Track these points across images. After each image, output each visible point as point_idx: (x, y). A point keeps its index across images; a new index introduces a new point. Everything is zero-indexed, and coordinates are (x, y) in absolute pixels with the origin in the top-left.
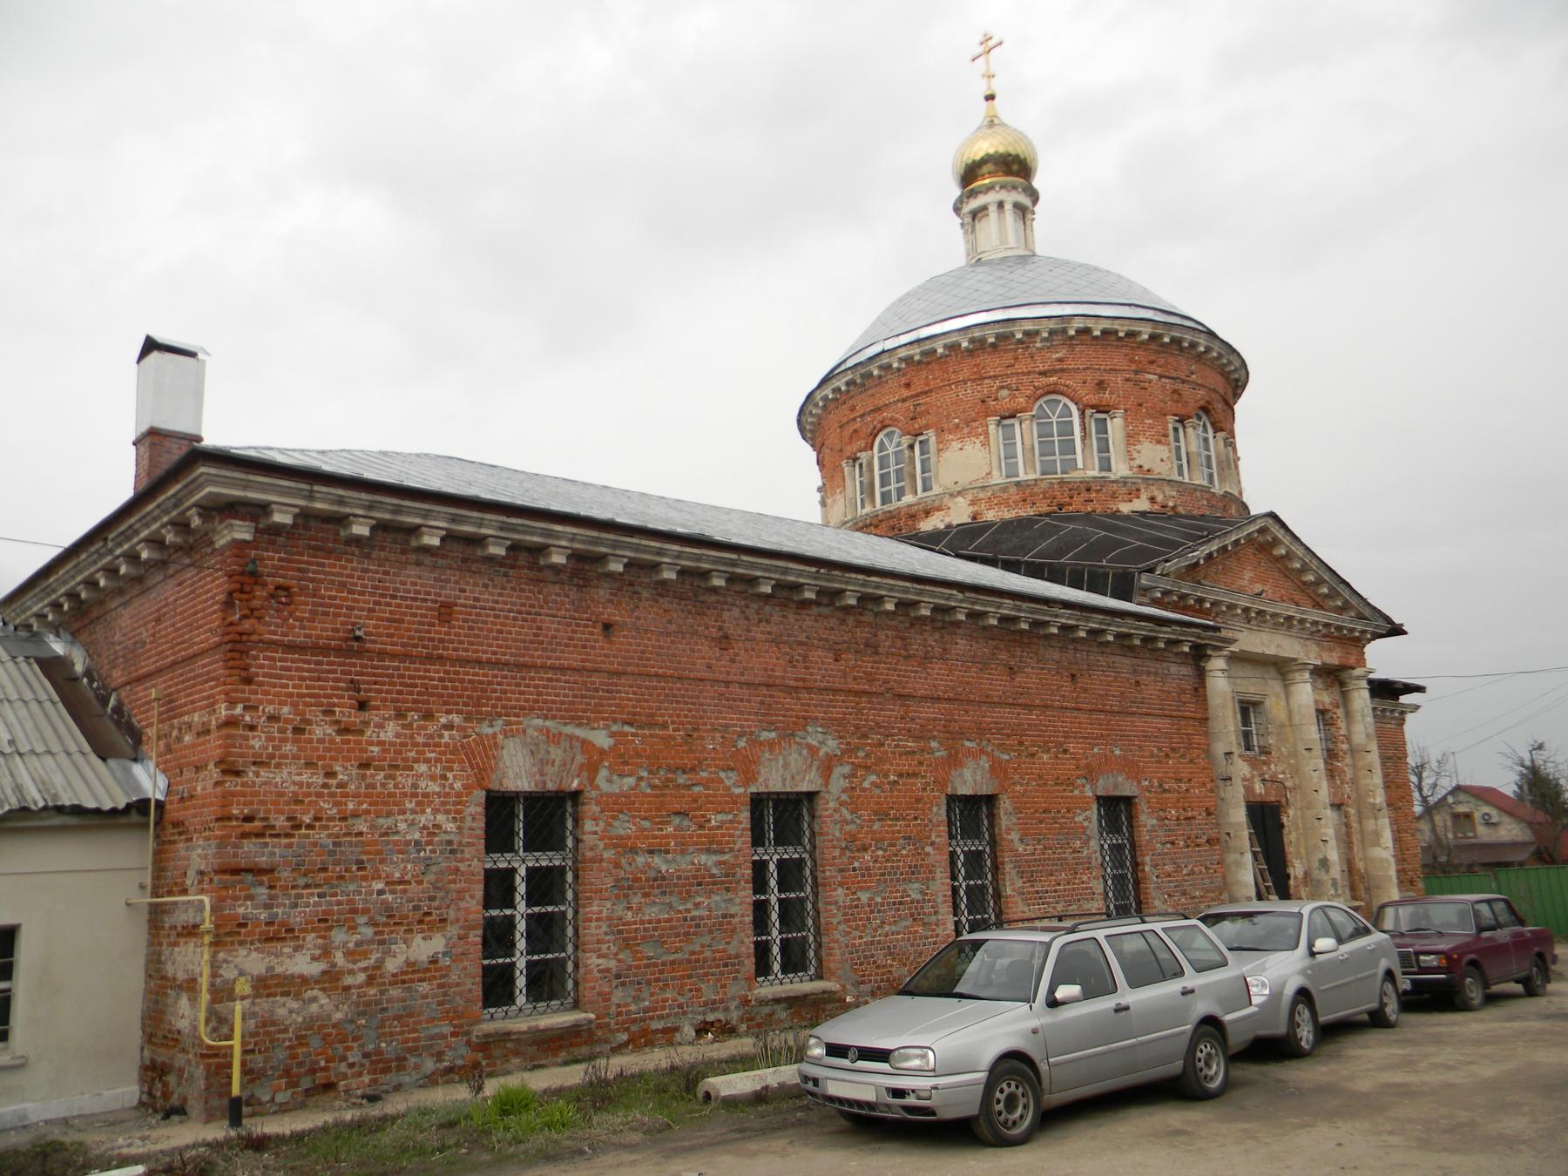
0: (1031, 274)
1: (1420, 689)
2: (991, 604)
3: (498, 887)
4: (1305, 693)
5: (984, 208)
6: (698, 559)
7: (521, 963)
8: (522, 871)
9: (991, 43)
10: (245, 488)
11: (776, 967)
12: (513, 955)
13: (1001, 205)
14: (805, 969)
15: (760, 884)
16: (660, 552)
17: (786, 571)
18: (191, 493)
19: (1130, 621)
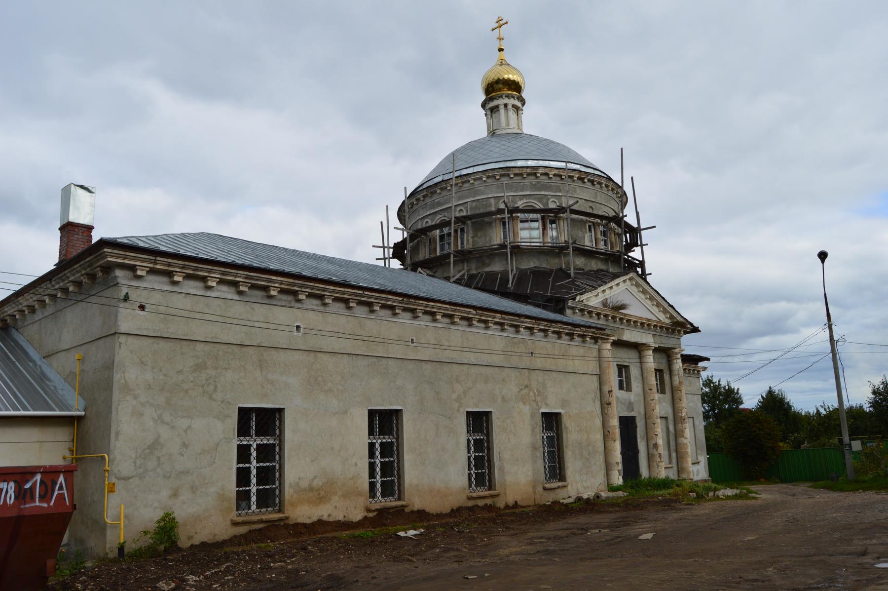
0: (519, 144)
1: (708, 359)
2: (490, 316)
3: (243, 453)
4: (651, 361)
5: (497, 107)
6: (343, 293)
7: (254, 489)
8: (255, 446)
9: (501, 22)
10: (124, 258)
11: (379, 494)
12: (249, 486)
13: (506, 105)
14: (393, 495)
15: (372, 454)
16: (324, 290)
17: (387, 299)
18: (98, 261)
19: (560, 325)
